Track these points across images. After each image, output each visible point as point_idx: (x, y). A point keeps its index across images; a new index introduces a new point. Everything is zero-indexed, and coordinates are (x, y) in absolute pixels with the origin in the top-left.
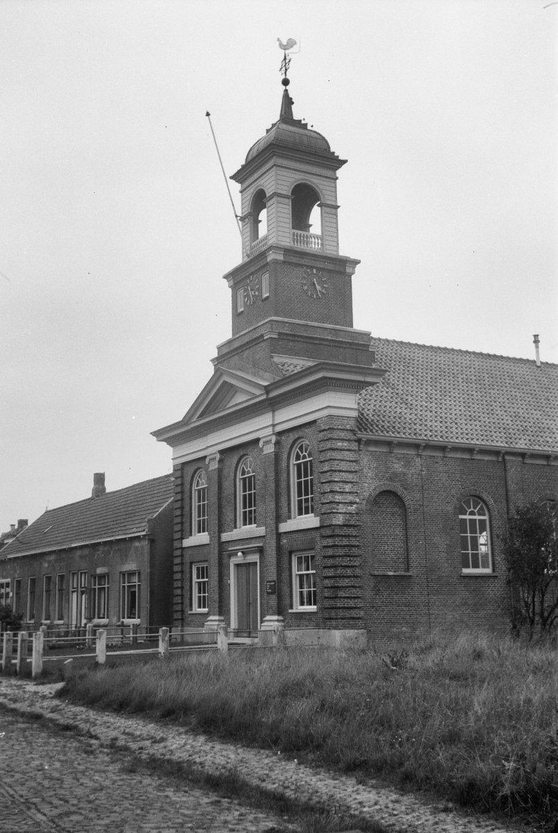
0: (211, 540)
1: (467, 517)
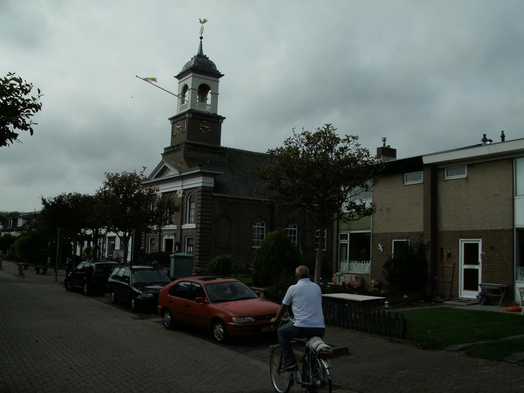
0: (424, 229)
1: (289, 229)
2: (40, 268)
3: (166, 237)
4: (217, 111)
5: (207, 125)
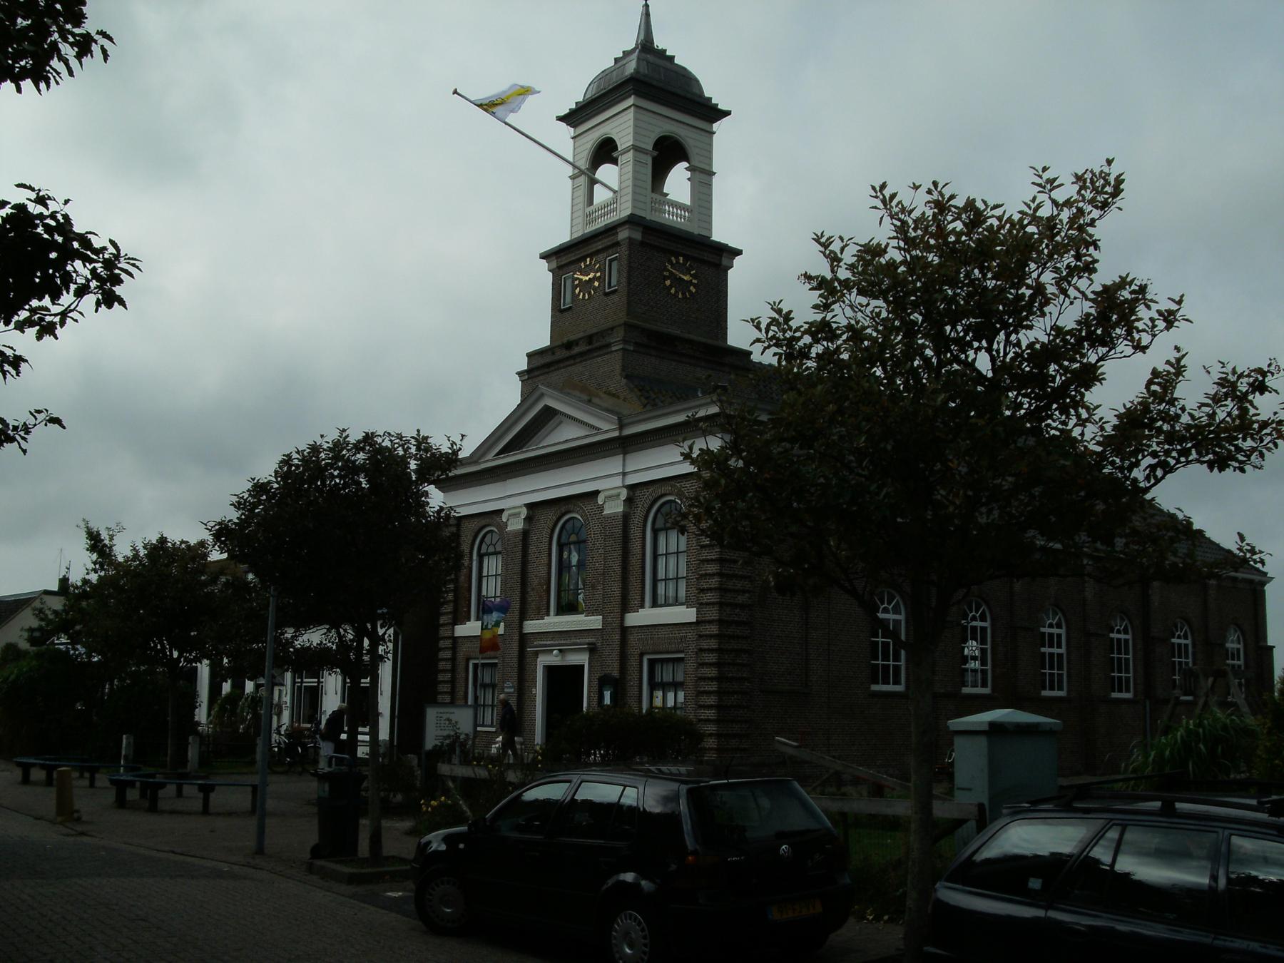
2: (34, 765)
3: (543, 660)
4: (710, 230)
5: (687, 272)
